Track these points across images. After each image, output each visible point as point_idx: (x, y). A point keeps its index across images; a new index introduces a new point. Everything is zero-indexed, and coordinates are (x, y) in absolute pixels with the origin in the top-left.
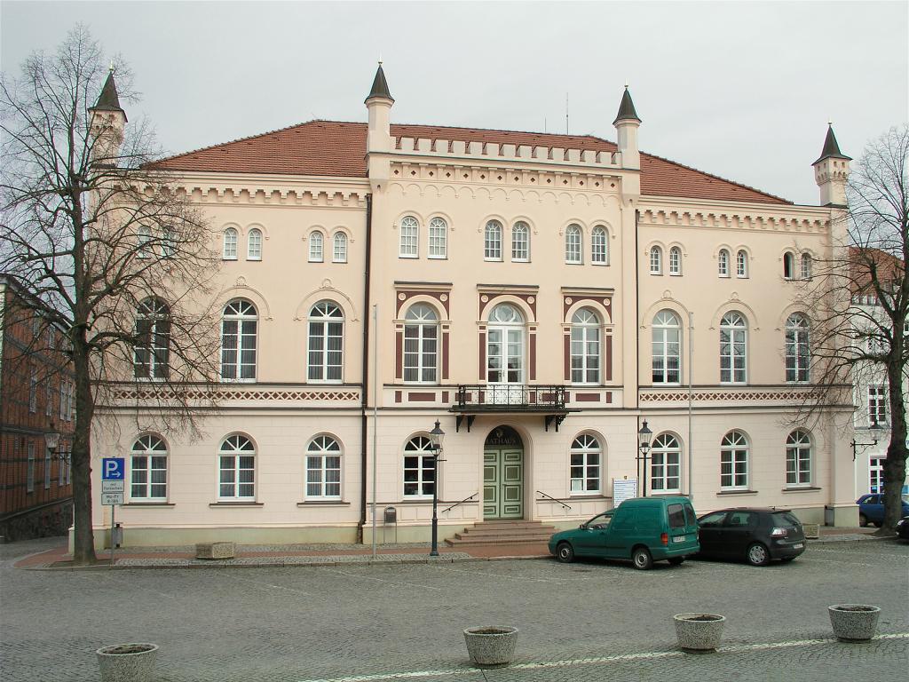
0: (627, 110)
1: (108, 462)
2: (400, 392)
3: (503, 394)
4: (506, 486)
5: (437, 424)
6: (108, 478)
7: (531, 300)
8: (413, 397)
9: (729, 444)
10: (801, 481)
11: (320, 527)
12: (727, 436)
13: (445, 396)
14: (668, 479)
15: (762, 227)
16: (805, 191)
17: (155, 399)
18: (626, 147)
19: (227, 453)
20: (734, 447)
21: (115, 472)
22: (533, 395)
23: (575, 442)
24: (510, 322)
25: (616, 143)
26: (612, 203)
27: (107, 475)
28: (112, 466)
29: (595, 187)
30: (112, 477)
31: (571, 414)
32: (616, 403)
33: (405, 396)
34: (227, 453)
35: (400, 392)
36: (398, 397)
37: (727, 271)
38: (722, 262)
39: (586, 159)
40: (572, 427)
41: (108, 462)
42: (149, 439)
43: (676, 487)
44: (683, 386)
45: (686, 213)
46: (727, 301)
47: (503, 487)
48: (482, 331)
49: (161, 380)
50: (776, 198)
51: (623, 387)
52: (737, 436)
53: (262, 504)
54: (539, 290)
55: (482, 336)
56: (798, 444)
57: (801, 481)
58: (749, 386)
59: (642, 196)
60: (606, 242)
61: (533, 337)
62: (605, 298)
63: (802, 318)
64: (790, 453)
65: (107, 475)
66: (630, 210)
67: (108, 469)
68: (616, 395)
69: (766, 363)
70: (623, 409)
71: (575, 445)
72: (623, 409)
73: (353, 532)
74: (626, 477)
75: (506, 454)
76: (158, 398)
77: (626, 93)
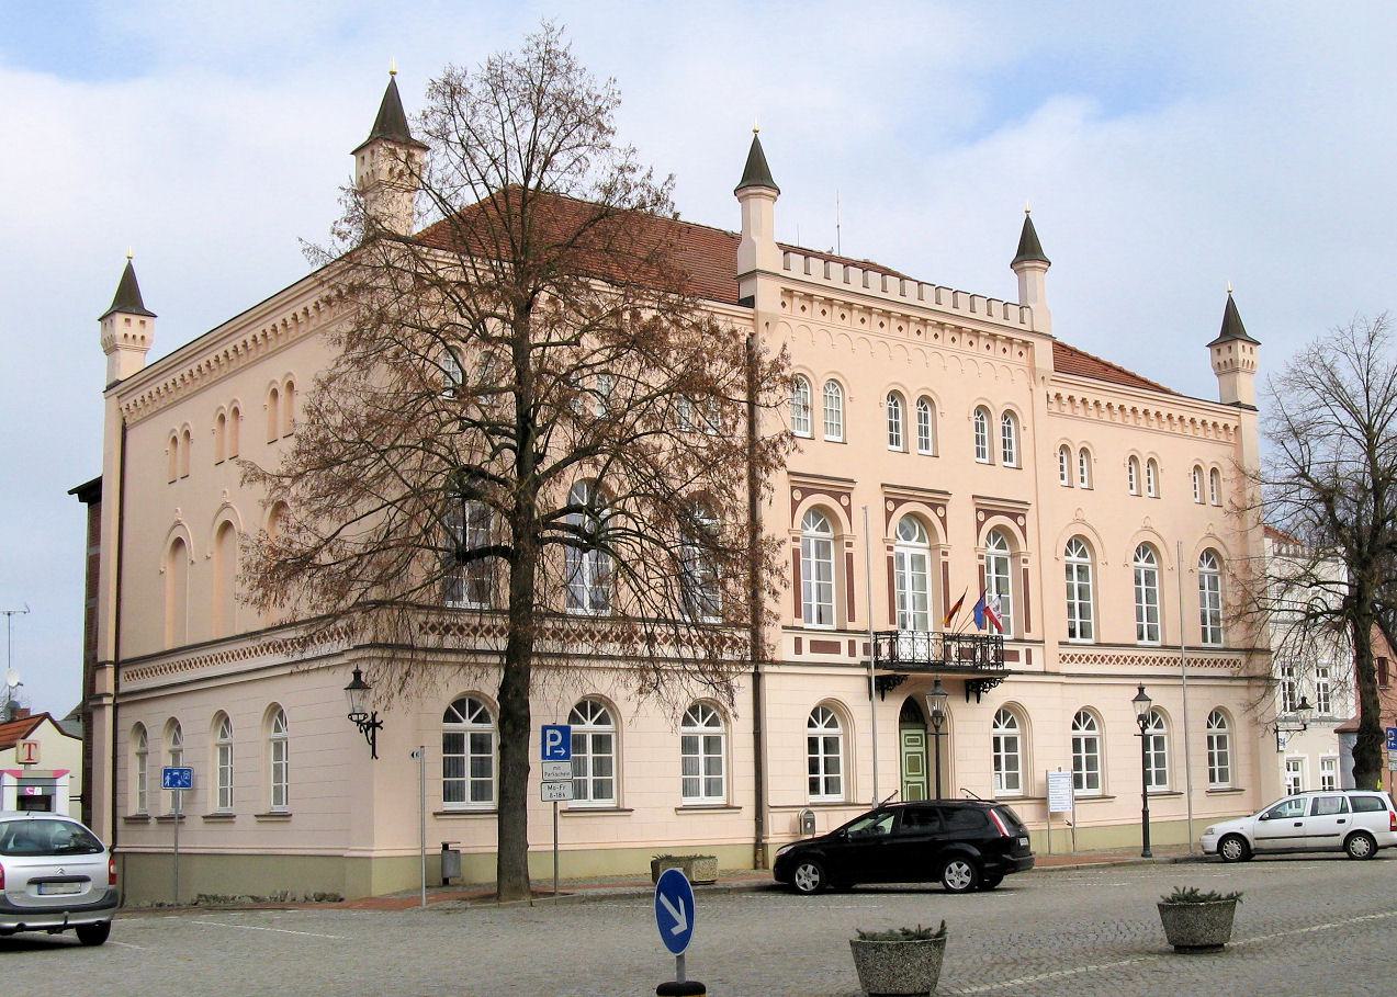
0: (756, 174)
1: (549, 732)
2: (854, 641)
3: (916, 648)
4: (908, 782)
5: (357, 674)
6: (549, 758)
7: (941, 511)
8: (817, 647)
9: (457, 720)
10: (474, 798)
11: (1093, 827)
12: (454, 704)
13: (852, 644)
14: (826, 778)
15: (1183, 430)
16: (1192, 371)
17: (490, 639)
18: (1035, 301)
19: (452, 727)
20: (1082, 732)
21: (558, 748)
22: (947, 649)
23: (449, 710)
24: (913, 542)
25: (736, 228)
26: (1022, 380)
27: (548, 754)
28: (554, 738)
29: (859, 325)
30: (554, 757)
31: (1011, 677)
32: (1037, 666)
33: (806, 646)
34: (452, 727)
35: (854, 641)
36: (798, 650)
37: (1134, 487)
38: (796, 416)
39: (870, 286)
40: (997, 696)
41: (549, 732)
42: (592, 707)
43: (719, 794)
44: (1098, 645)
45: (1096, 401)
46: (1139, 528)
47: (904, 784)
48: (890, 553)
49: (475, 606)
50: (1146, 382)
51: (1043, 642)
52: (474, 706)
53: (631, 810)
54: (951, 498)
55: (890, 559)
56: (700, 729)
57: (474, 798)
58: (1164, 647)
59: (1057, 374)
60: (986, 429)
61: (946, 565)
62: (940, 505)
63: (1210, 555)
64: (688, 744)
65: (548, 754)
66: (1041, 390)
67: (549, 744)
68: (1036, 651)
69: (1180, 616)
70: (1045, 673)
71: (449, 717)
72: (1045, 673)
73: (750, 851)
74: (1060, 769)
75: (906, 735)
76: (495, 636)
77: (1028, 223)
